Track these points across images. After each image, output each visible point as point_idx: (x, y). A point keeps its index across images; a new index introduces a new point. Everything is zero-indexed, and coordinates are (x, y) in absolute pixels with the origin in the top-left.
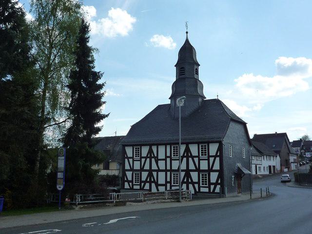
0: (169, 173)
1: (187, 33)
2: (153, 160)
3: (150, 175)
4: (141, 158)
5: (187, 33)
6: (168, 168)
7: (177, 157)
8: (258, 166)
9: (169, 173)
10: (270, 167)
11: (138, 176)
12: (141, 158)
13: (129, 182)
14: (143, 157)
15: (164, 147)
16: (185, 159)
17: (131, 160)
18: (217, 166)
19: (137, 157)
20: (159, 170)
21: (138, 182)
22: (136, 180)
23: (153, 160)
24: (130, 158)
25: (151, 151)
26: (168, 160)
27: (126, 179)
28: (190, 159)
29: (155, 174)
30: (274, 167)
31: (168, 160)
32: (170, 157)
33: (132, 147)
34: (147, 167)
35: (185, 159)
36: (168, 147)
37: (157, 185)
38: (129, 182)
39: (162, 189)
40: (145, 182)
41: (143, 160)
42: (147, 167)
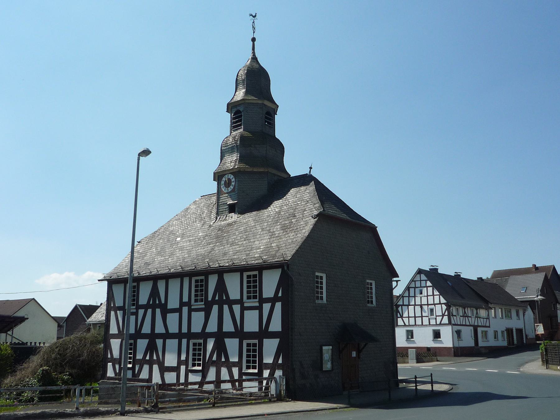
0: (184, 341)
1: (254, 40)
2: (158, 311)
3: (151, 348)
4: (263, 301)
5: (254, 40)
6: (185, 330)
7: (201, 305)
8: (480, 330)
9: (184, 341)
10: (509, 331)
11: (254, 351)
12: (263, 301)
13: (114, 361)
14: (268, 300)
15: (179, 280)
16: (215, 308)
17: (237, 308)
18: (276, 325)
19: (252, 300)
20: (167, 336)
21: (254, 368)
22: (248, 362)
23: (158, 311)
24: (236, 302)
25: (154, 293)
26: (185, 310)
27: (109, 356)
28: (226, 307)
29: (159, 342)
30: (519, 331)
31: (185, 310)
32: (188, 304)
33: (238, 275)
34: (146, 329)
35: (215, 308)
36: (186, 281)
37: (164, 370)
38: (114, 361)
39: (170, 378)
40: (142, 362)
41: (267, 307)
42: (146, 329)
